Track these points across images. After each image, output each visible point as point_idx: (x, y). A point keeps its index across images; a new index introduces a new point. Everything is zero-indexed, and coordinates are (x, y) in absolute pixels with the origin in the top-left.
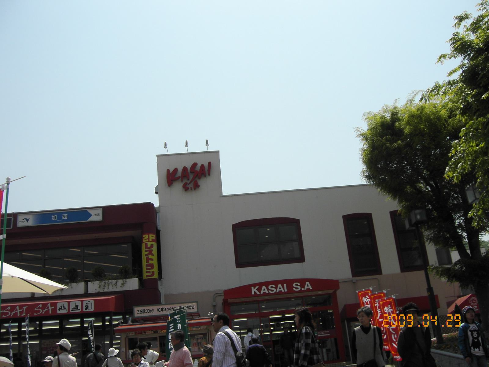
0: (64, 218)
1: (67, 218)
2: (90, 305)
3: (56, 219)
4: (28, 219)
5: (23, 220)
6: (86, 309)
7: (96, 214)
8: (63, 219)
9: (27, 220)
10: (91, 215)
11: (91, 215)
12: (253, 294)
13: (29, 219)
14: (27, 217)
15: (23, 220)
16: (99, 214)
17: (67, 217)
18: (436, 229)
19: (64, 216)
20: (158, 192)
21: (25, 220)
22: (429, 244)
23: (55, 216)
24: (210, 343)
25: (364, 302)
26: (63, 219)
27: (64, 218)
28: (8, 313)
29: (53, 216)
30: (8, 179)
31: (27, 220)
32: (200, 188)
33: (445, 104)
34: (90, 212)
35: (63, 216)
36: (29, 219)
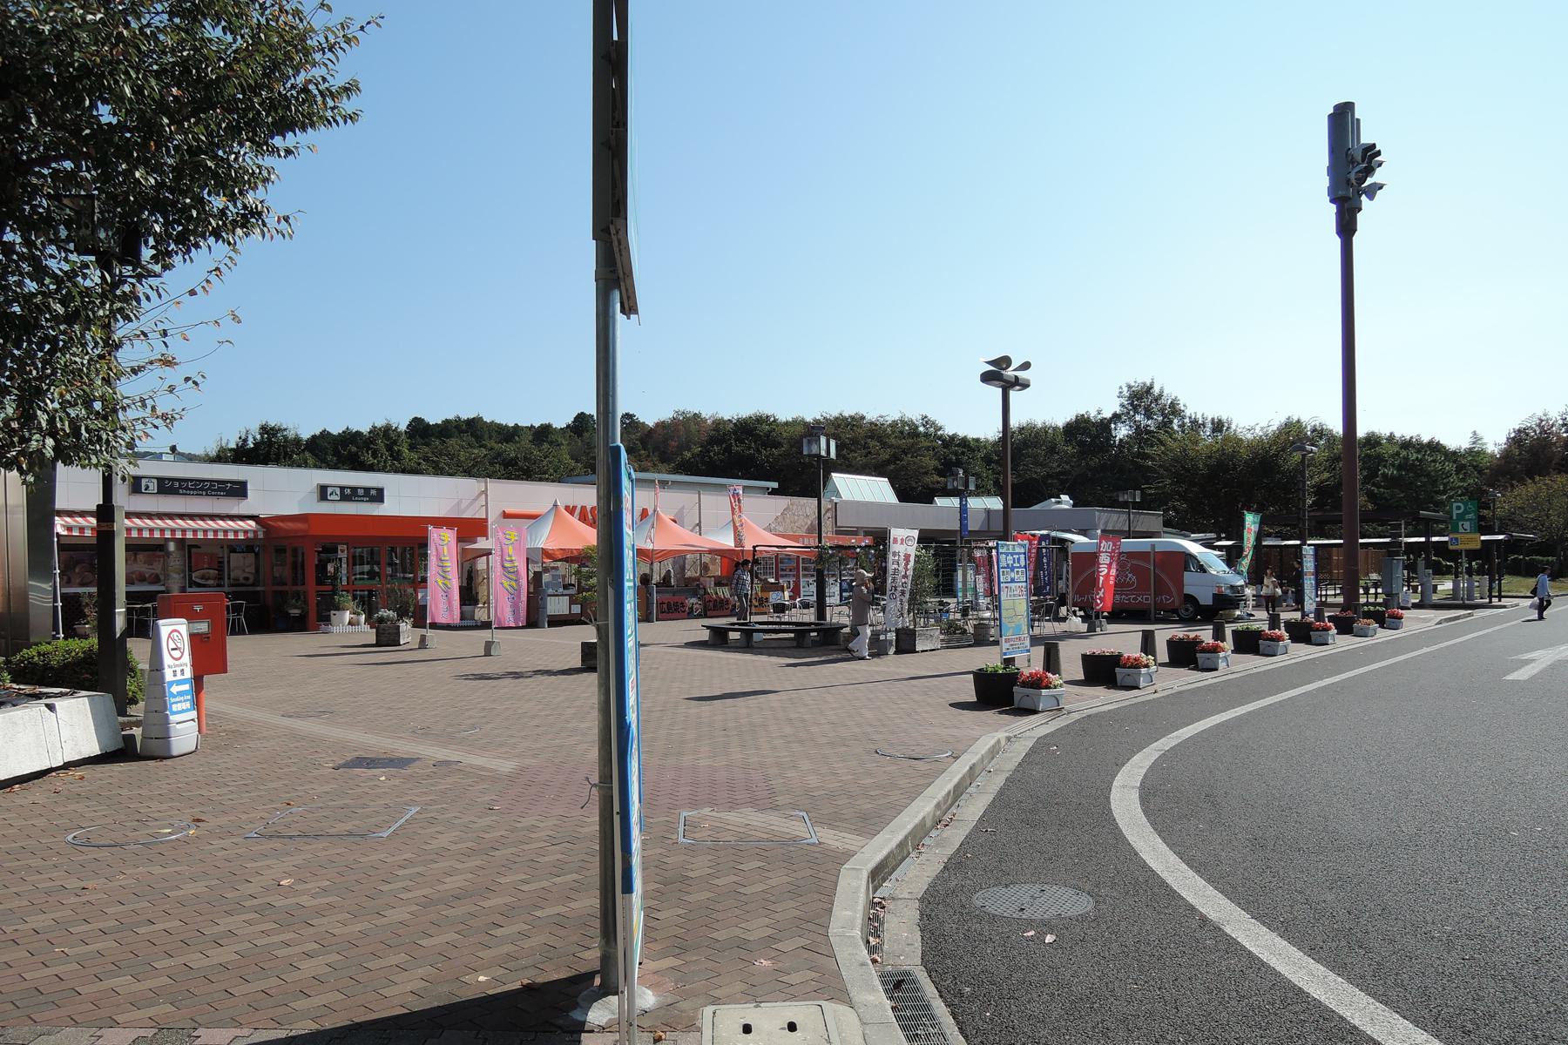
2: (150, 485)
6: (146, 489)
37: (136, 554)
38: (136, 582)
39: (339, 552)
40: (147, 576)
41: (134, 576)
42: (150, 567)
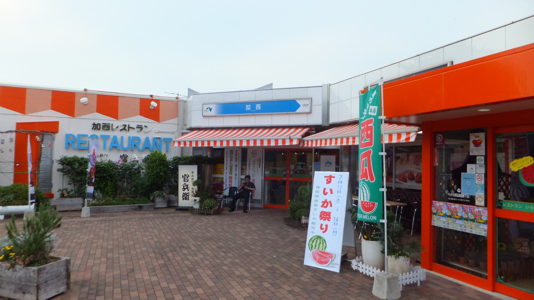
0: (258, 108)
1: (260, 109)
3: (250, 109)
4: (211, 108)
5: (207, 109)
7: (304, 105)
8: (256, 109)
9: (211, 110)
10: (300, 106)
11: (300, 106)
12: (212, 175)
13: (212, 108)
14: (211, 106)
15: (207, 109)
16: (308, 105)
17: (260, 107)
18: (142, 175)
19: (258, 106)
20: (58, 171)
21: (208, 109)
22: (59, 165)
23: (249, 105)
24: (517, 198)
25: (353, 200)
26: (256, 109)
27: (258, 108)
28: (370, 150)
29: (247, 106)
30: (68, 184)
31: (211, 110)
32: (58, 168)
33: (152, 162)
34: (298, 102)
35: (256, 106)
36: (212, 108)
37: (408, 155)
38: (407, 179)
39: (472, 146)
40: (415, 175)
41: (407, 175)
42: (418, 167)
